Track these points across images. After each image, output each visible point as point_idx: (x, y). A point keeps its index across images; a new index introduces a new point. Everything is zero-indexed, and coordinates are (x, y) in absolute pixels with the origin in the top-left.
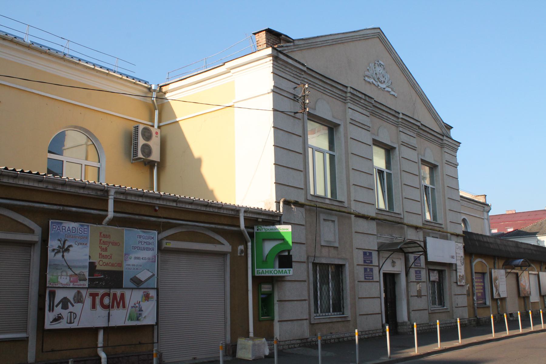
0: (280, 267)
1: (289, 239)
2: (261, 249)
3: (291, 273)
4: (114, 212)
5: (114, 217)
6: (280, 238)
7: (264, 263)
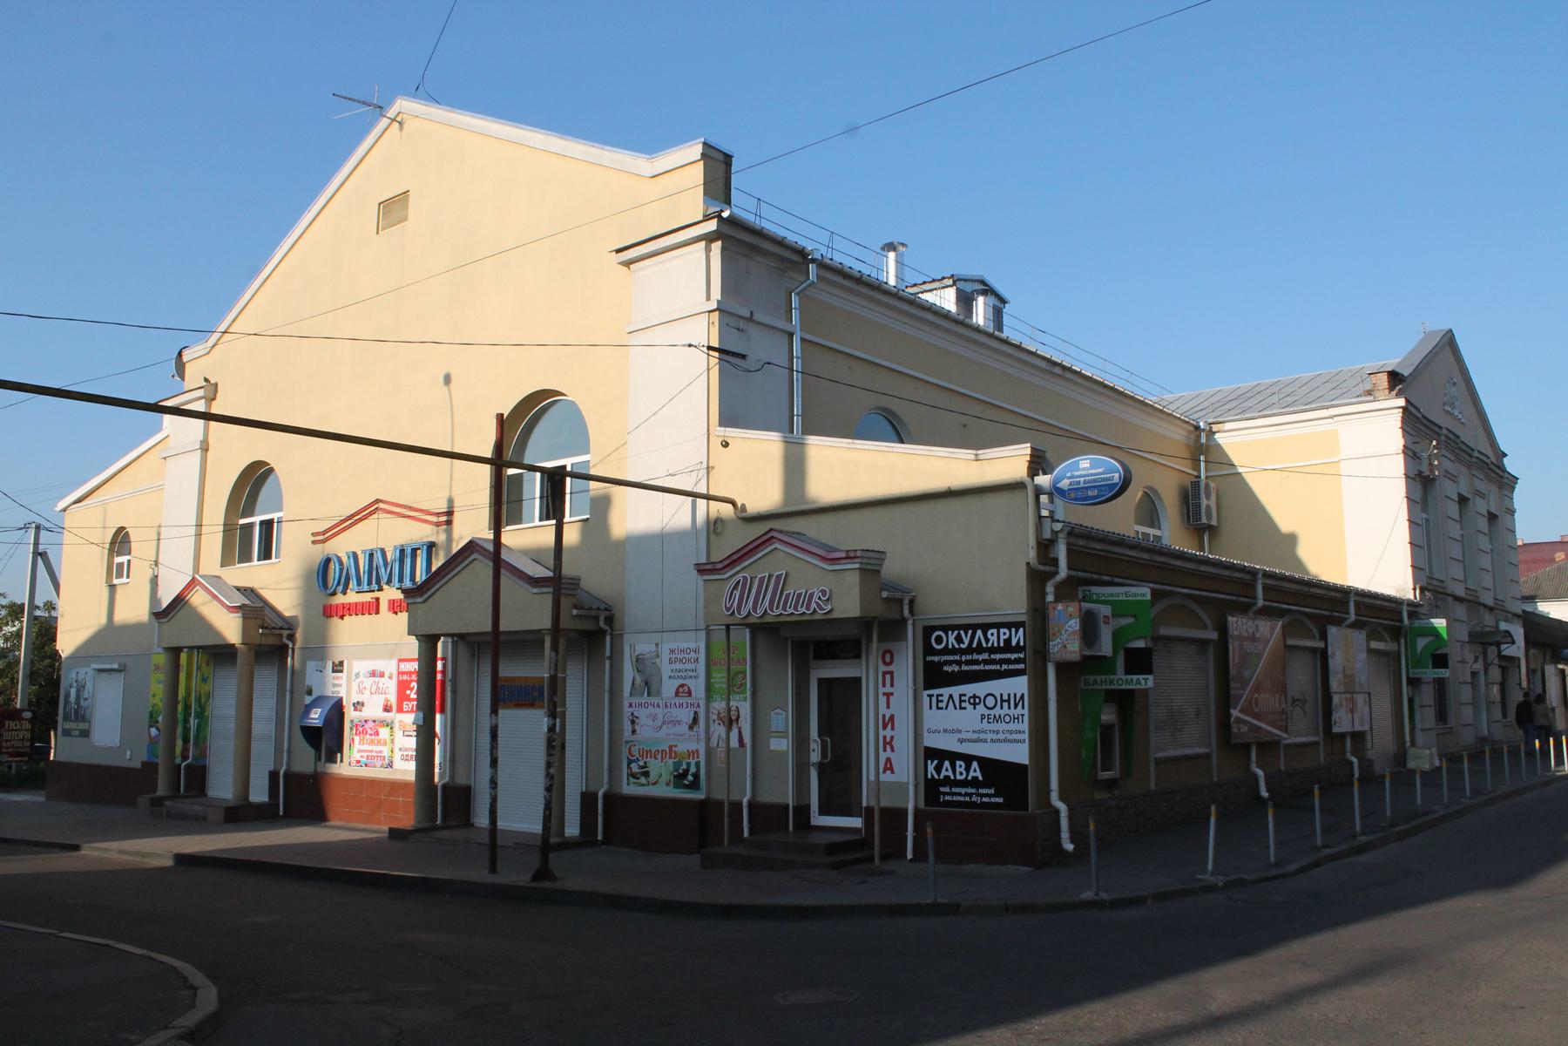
0: (1128, 672)
1: (1444, 634)
2: (1415, 647)
3: (1150, 684)
4: (1069, 568)
5: (1069, 577)
6: (1434, 633)
7: (1418, 663)
